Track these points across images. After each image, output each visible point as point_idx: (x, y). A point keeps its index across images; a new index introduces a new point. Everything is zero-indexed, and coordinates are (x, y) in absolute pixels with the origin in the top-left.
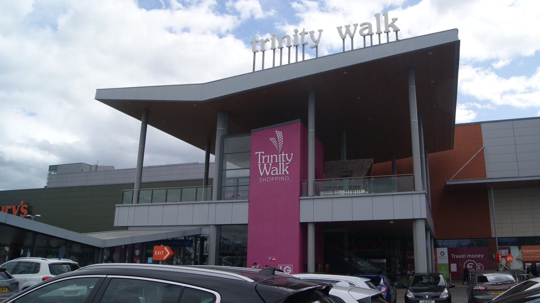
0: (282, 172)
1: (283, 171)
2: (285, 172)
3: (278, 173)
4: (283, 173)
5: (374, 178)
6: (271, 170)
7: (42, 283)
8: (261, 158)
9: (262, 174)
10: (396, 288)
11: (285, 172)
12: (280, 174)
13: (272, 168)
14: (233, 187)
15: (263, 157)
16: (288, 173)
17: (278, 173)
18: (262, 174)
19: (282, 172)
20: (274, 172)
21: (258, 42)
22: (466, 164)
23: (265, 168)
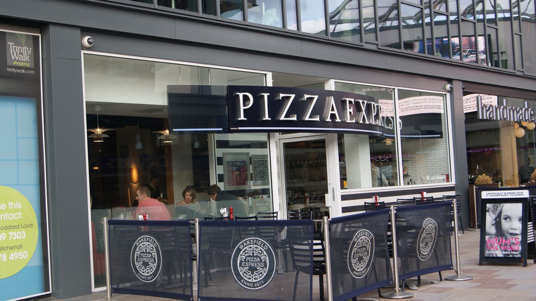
0: (25, 59)
1: (26, 58)
2: (27, 59)
3: (23, 59)
4: (26, 60)
6: (19, 57)
8: (12, 48)
9: (13, 58)
11: (27, 59)
12: (24, 60)
13: (20, 55)
15: (13, 46)
16: (29, 60)
17: (23, 59)
18: (13, 58)
19: (25, 59)
20: (21, 58)
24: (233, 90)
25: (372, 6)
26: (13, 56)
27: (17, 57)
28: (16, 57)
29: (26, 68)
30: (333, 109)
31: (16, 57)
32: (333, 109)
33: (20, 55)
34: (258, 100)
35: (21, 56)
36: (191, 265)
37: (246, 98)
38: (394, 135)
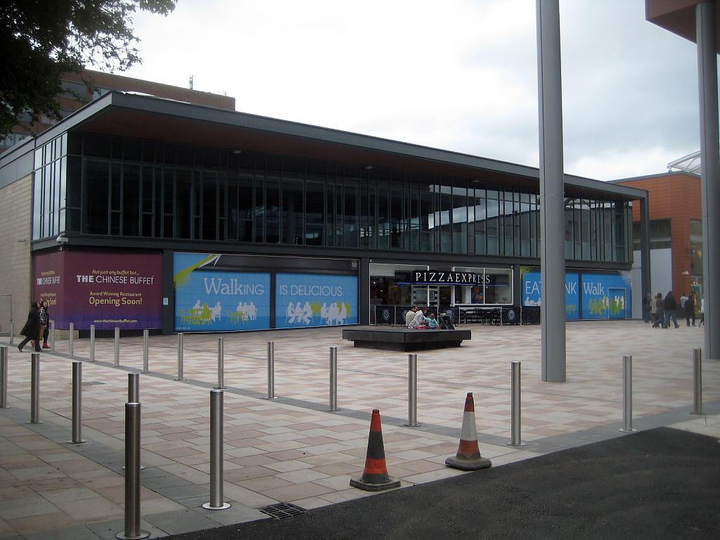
0: (234, 292)
1: (236, 290)
2: (238, 292)
3: (230, 292)
4: (236, 293)
5: (222, 214)
6: (221, 288)
7: (278, 338)
9: (208, 292)
10: (72, 133)
11: (238, 292)
13: (223, 285)
14: (488, 200)
18: (208, 292)
19: (234, 292)
20: (225, 291)
21: (24, 127)
22: (112, 321)
23: (213, 283)
24: (415, 272)
25: (88, 384)
26: (209, 288)
27: (217, 288)
28: (215, 289)
29: (648, 217)
30: (535, 287)
31: (215, 289)
32: (535, 287)
33: (223, 285)
34: (423, 275)
35: (224, 286)
36: (352, 413)
37: (419, 275)
38: (143, 215)
